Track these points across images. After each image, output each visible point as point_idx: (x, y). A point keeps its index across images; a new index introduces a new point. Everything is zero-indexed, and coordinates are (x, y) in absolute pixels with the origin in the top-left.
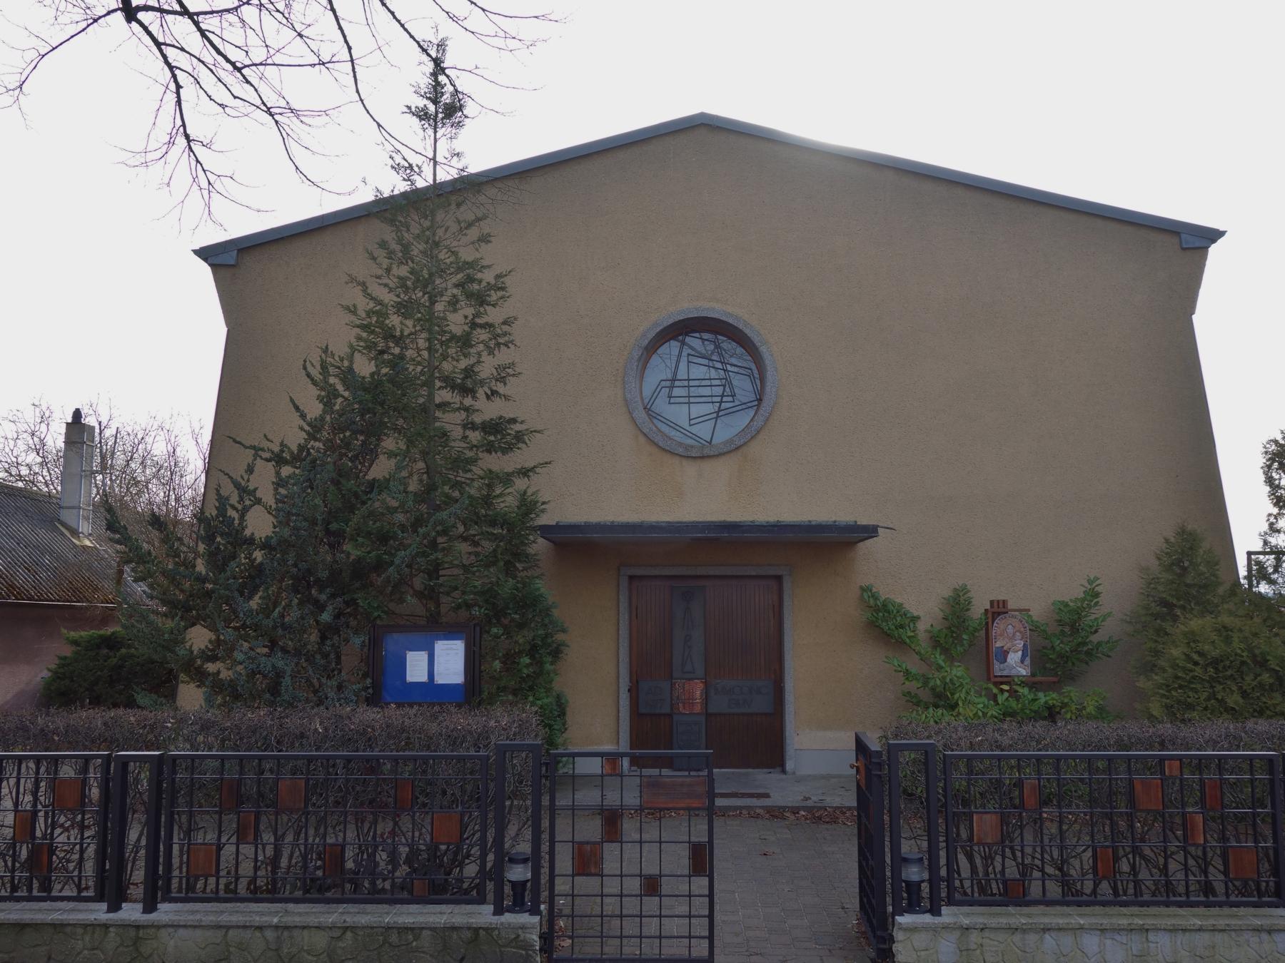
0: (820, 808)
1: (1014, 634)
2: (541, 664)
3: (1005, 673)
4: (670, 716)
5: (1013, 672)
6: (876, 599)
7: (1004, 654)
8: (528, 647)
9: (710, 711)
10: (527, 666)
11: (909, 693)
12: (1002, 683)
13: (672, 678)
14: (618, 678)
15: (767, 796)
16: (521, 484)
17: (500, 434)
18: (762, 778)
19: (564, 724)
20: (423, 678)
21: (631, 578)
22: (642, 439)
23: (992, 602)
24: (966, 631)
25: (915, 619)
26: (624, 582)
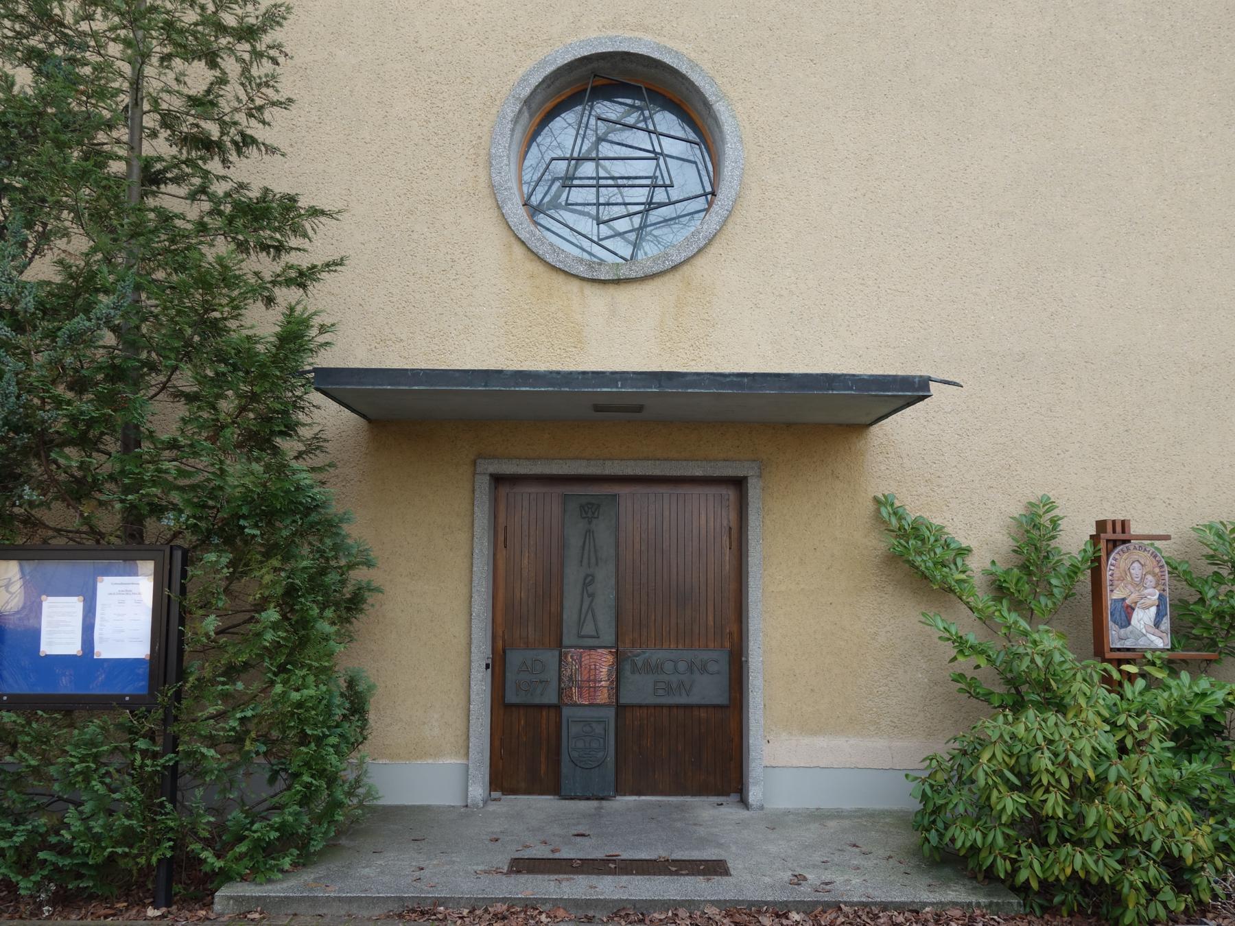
0: (827, 906)
1: (1143, 579)
2: (305, 623)
3: (1128, 644)
4: (557, 708)
5: (1142, 643)
6: (901, 518)
7: (1126, 613)
8: (279, 590)
9: (623, 701)
10: (275, 626)
11: (962, 676)
12: (1128, 662)
13: (560, 645)
14: (470, 644)
15: (716, 868)
16: (286, 296)
17: (266, 219)
18: (710, 813)
19: (363, 728)
20: (73, 647)
21: (498, 480)
22: (518, 250)
23: (1101, 525)
24: (1053, 576)
25: (964, 552)
26: (484, 484)
